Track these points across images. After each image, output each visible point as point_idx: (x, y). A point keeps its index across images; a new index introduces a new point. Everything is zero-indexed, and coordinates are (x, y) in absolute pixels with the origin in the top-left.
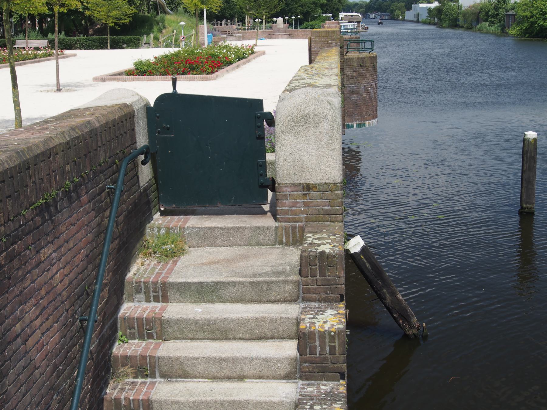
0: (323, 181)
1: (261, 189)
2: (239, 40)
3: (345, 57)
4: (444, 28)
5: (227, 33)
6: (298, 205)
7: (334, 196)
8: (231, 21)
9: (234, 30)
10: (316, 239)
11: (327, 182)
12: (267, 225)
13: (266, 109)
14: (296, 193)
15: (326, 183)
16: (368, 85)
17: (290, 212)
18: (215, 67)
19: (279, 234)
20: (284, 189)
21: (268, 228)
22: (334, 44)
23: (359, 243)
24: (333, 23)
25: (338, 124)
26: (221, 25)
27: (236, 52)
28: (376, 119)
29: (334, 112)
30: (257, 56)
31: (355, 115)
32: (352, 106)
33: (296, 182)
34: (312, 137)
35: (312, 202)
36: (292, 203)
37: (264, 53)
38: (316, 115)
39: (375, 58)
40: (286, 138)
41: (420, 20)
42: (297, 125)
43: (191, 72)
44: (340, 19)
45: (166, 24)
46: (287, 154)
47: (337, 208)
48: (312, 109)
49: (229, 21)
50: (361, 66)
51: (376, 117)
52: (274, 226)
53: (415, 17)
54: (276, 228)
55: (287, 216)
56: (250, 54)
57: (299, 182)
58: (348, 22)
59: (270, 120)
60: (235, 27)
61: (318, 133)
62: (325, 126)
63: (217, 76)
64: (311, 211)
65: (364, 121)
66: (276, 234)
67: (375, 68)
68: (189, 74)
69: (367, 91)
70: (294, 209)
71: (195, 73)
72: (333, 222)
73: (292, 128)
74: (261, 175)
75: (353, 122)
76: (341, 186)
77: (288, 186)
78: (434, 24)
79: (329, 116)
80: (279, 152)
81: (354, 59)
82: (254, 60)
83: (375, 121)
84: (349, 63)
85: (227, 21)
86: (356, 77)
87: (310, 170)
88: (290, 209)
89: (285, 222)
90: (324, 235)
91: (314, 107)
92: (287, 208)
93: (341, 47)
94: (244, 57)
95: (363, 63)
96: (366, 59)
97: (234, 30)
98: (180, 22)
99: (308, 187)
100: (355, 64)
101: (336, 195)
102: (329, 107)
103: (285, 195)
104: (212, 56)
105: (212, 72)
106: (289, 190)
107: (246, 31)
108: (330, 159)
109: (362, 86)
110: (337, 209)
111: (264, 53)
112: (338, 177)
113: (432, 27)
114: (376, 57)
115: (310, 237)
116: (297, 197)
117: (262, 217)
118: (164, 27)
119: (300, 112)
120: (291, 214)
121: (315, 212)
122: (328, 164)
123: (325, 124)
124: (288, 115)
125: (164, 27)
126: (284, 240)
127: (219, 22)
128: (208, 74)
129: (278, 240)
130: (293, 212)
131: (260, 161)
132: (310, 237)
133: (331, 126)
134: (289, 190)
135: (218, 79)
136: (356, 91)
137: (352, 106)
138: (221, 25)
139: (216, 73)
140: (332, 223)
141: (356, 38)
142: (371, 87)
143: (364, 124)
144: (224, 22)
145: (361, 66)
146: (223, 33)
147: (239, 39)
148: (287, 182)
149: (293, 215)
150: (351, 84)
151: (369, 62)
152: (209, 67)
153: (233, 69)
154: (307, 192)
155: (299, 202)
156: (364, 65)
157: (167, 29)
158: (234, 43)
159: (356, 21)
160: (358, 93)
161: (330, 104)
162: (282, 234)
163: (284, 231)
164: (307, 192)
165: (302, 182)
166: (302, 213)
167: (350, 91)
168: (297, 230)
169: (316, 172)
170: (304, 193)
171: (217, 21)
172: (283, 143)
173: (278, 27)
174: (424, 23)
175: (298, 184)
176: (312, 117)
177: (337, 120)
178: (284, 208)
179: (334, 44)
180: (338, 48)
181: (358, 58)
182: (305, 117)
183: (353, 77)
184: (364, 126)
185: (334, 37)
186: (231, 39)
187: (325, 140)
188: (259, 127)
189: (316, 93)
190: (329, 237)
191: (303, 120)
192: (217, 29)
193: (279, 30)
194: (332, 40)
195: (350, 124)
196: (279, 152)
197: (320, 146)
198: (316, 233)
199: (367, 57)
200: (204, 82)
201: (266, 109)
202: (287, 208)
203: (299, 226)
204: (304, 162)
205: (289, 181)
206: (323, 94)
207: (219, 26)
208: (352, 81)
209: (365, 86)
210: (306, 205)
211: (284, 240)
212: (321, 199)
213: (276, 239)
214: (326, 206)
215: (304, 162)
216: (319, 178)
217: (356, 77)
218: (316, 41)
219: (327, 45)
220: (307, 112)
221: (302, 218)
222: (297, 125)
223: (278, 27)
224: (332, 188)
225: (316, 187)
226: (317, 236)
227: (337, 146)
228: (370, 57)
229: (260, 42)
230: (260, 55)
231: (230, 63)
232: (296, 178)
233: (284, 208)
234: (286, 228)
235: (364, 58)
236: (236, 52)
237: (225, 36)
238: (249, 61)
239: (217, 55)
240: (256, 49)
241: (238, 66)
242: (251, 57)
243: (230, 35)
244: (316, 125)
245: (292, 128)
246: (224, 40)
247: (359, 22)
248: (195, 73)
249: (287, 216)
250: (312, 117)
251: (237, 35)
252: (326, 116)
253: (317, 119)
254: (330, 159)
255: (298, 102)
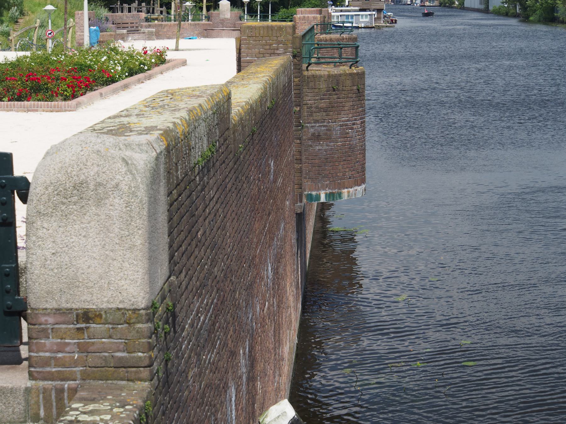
0: (113, 306)
1: (8, 318)
2: (149, 39)
3: (306, 73)
4: (533, 22)
5: (129, 25)
6: (67, 349)
7: (134, 333)
8: (148, 3)
9: (141, 21)
10: (85, 413)
11: (121, 306)
12: (10, 386)
13: (18, 172)
14: (64, 326)
15: (119, 309)
16: (346, 125)
17: (53, 362)
18: (80, 87)
19: (33, 402)
20: (43, 319)
21: (12, 391)
22: (281, 51)
23: (284, 413)
24: (310, 12)
25: (141, 201)
26: (130, 11)
27: (125, 62)
28: (363, 186)
29: (134, 178)
30: (168, 69)
31: (324, 177)
32: (317, 161)
33: (64, 305)
34: (93, 223)
35: (93, 343)
36: (57, 344)
37: (184, 63)
38: (100, 184)
39: (361, 76)
40: (45, 225)
41: (491, 8)
42: (65, 201)
43: (33, 95)
44: (347, 3)
45: (26, 9)
46: (48, 254)
47: (140, 354)
48: (92, 173)
49: (144, 4)
50: (334, 90)
51: (363, 181)
52: (23, 386)
53: (481, 3)
54: (28, 390)
55: (48, 369)
56: (157, 65)
57: (69, 306)
58: (361, 10)
59: (23, 187)
60: (143, 15)
61: (103, 217)
62: (116, 204)
63: (78, 105)
64: (91, 360)
65: (339, 189)
66: (27, 401)
67: (360, 93)
68: (28, 100)
69: (344, 135)
70: (60, 355)
71: (39, 97)
72: (132, 381)
73: (55, 207)
74: (8, 292)
75: (318, 190)
76: (147, 314)
77: (48, 314)
78: (515, 16)
79: (124, 187)
80: (32, 251)
81: (321, 76)
82: (160, 77)
83: (360, 189)
84: (311, 84)
85: (140, 4)
86: (326, 110)
87: (90, 284)
88: (53, 355)
89: (44, 379)
90: (105, 406)
91: (96, 169)
92: (47, 354)
93: (294, 56)
94: (142, 71)
95: (338, 84)
96: (343, 78)
97: (141, 21)
98: (46, 5)
99: (86, 316)
100: (323, 86)
101: (138, 332)
102: (124, 169)
103: (45, 330)
104: (82, 67)
105: (74, 97)
106: (51, 320)
107: (173, 22)
108: (126, 264)
109: (336, 128)
110: (140, 357)
111: (184, 63)
112: (140, 299)
113: (513, 22)
114: (363, 74)
115: (77, 409)
116: (65, 333)
117: (9, 369)
118: (22, 13)
119: (69, 176)
120: (56, 366)
121: (99, 362)
122: (122, 274)
123: (117, 201)
124: (48, 182)
125: (22, 13)
126: (42, 413)
127: (126, 6)
128: (65, 100)
129: (31, 412)
130: (59, 362)
131: (7, 268)
132: (77, 409)
133: (128, 204)
134: (51, 320)
135: (80, 109)
136: (326, 134)
137: (317, 161)
138: (130, 11)
139: (80, 99)
140: (131, 383)
141: (350, 39)
142: (352, 129)
143: (340, 195)
144: (135, 5)
145: (334, 90)
146: (119, 25)
147: (150, 37)
148: (48, 306)
149: (59, 366)
150: (316, 121)
151: (349, 83)
152: (69, 86)
153: (115, 91)
154: (83, 325)
155: (69, 344)
156: (341, 88)
157: (27, 18)
158: (135, 45)
159: (373, 7)
160: (329, 138)
161: (127, 164)
162: (37, 403)
163: (41, 396)
164: (83, 325)
165: (74, 306)
166: (76, 363)
167: (313, 135)
168: (66, 394)
169: (101, 287)
170: (78, 326)
171: (121, 4)
172: (40, 233)
173: (222, 17)
174: (499, 13)
175: (67, 310)
176: (92, 187)
177: (139, 194)
178: (41, 354)
179: (281, 51)
180: (289, 56)
181: (329, 76)
182: (80, 186)
183: (319, 110)
184: (340, 197)
185: (282, 38)
186: (136, 36)
187: (117, 230)
188: (4, 204)
189: (103, 143)
190: (111, 409)
191: (75, 192)
192: (110, 19)
193: (223, 21)
194: (279, 43)
195: (314, 193)
196: (32, 251)
197: (107, 240)
198: (93, 400)
199: (346, 75)
200: (54, 113)
201: (18, 172)
202: (47, 354)
203: (69, 389)
204: (78, 269)
205: (52, 305)
206: (115, 146)
207: (134, 13)
208: (318, 116)
209: (341, 126)
210: (83, 349)
211: (42, 413)
212: (110, 337)
213: (26, 411)
214: (119, 351)
215: (78, 269)
216: (106, 299)
217: (326, 110)
218: (248, 44)
219: (269, 51)
220: (83, 177)
221: (75, 372)
222: (65, 201)
223: (222, 17)
224: (130, 319)
225: (100, 316)
226: (91, 407)
227: (139, 242)
228: (351, 74)
229: (184, 43)
230: (174, 67)
231: (113, 81)
232: (64, 299)
233: (41, 354)
234: (45, 390)
235: (340, 75)
236: (125, 62)
237: (125, 31)
238: (149, 78)
239: (90, 66)
240: (169, 56)
241: (126, 87)
242: (157, 69)
243: (134, 30)
244: (99, 201)
245: (55, 207)
246: (123, 38)
247: (379, 11)
248: (39, 97)
249: (48, 369)
250: (92, 187)
251: (146, 30)
252: (117, 185)
253: (101, 190)
254: (126, 264)
255: (67, 160)
